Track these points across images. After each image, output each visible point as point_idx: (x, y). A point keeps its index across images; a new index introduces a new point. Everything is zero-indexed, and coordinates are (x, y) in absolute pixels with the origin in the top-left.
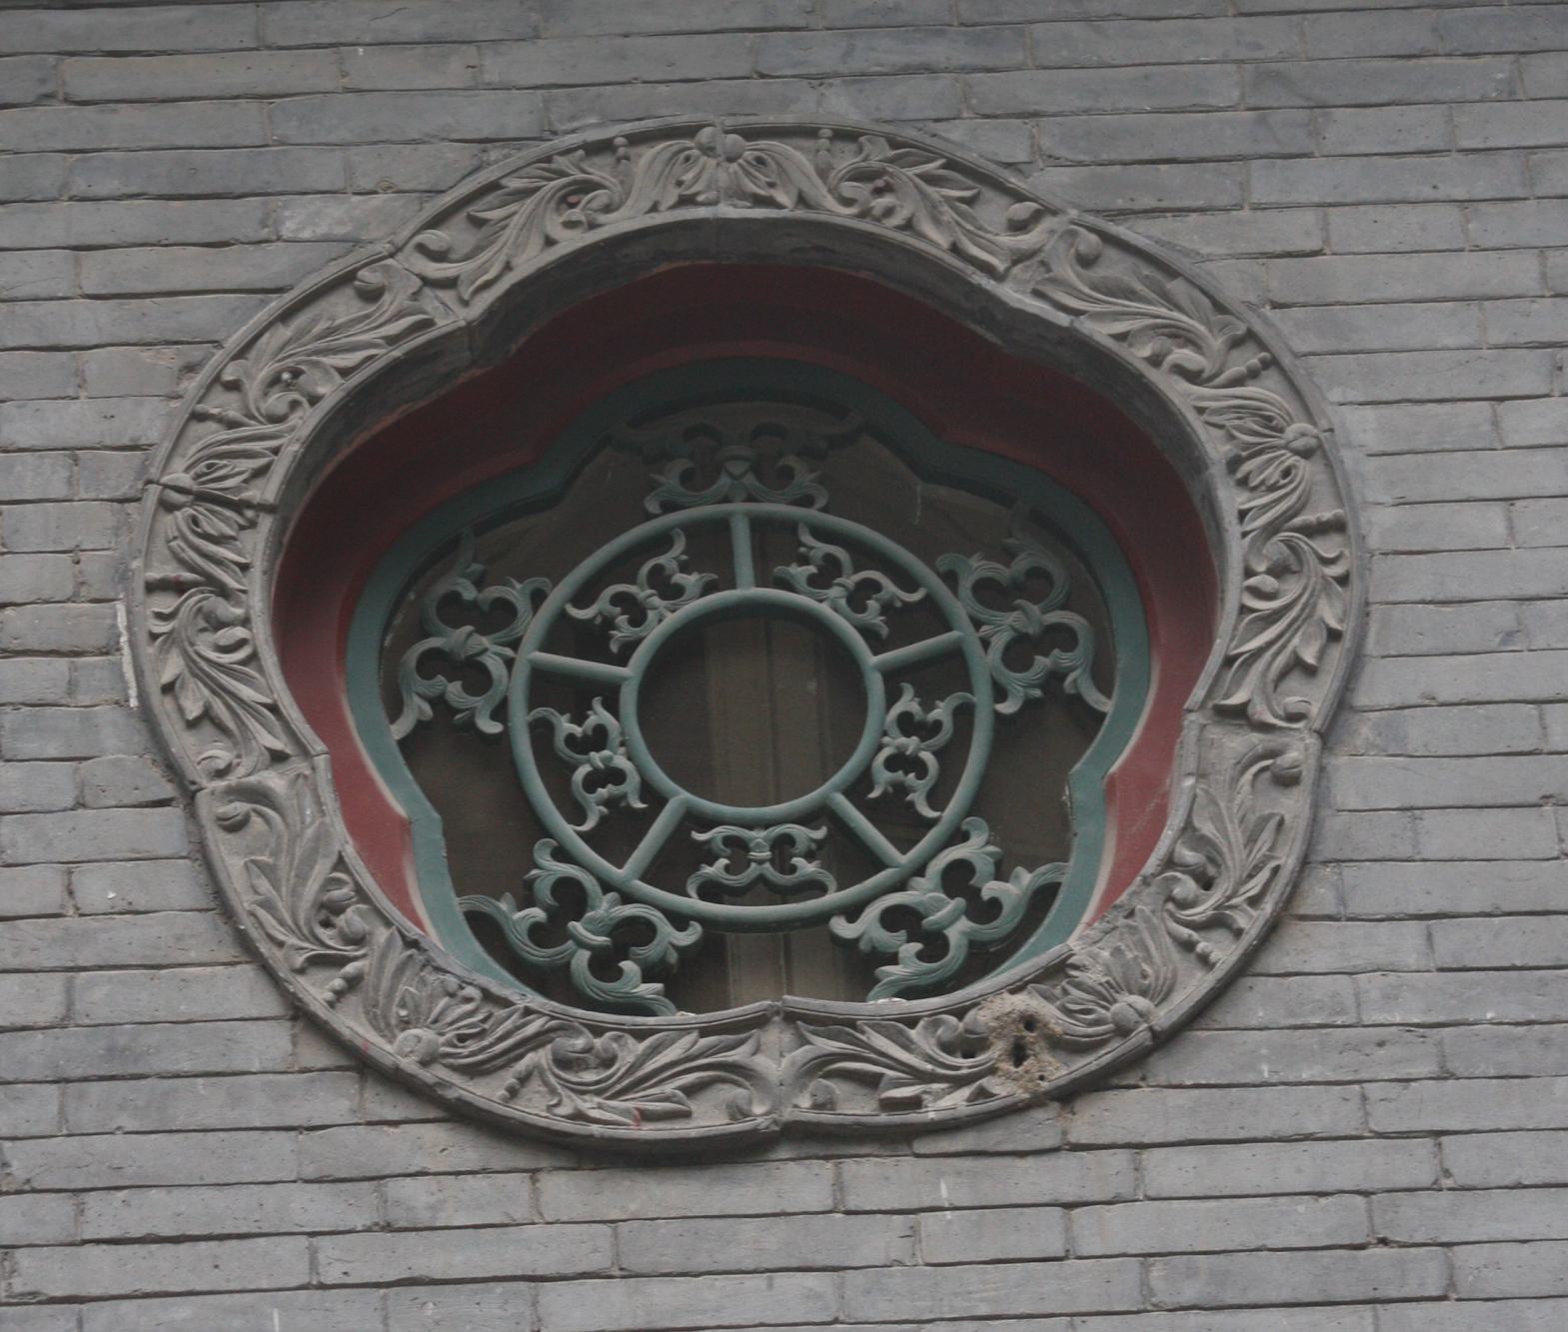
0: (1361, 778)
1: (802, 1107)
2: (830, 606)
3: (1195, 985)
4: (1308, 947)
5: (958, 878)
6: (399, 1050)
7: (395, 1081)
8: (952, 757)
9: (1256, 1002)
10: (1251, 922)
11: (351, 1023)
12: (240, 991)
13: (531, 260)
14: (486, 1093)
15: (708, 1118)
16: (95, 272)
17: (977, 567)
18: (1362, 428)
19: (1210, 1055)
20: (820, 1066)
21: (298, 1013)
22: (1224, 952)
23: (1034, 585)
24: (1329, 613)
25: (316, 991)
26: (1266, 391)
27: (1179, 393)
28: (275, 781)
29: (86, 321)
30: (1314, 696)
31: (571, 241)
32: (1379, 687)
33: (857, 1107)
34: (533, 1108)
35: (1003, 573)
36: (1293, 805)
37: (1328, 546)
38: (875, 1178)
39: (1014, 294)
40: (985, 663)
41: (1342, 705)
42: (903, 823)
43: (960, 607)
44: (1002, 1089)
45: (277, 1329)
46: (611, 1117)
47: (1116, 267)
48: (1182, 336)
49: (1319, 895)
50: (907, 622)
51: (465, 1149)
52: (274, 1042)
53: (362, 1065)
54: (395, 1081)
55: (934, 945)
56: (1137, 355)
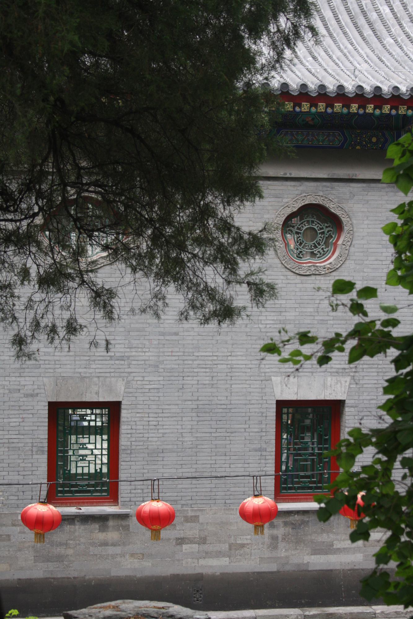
0: (352, 249)
1: (314, 273)
2: (315, 227)
3: (340, 265)
4: (347, 262)
5: (322, 249)
6: (288, 267)
7: (288, 269)
8: (323, 240)
9: (343, 266)
10: (343, 260)
11: (286, 265)
12: (277, 261)
13: (300, 205)
14: (294, 270)
15: (308, 273)
16: (270, 204)
17: (326, 225)
18: (355, 222)
19: (340, 270)
20: (315, 269)
21: (282, 263)
22: (342, 263)
23: (329, 227)
24: (351, 237)
25: (283, 262)
26: (348, 219)
27: (343, 219)
28: (281, 246)
29: (270, 208)
30: (349, 244)
31: (303, 204)
32: (353, 243)
33: (317, 273)
34: (297, 272)
35: (327, 225)
36: (347, 252)
37: (351, 232)
38: (318, 277)
39: (332, 211)
40: (326, 232)
41: (351, 244)
42: (319, 244)
43: (324, 228)
44: (327, 272)
45: (409, 368)
46: (302, 273)
47: (340, 209)
48: (343, 214)
49: (348, 258)
50: (321, 229)
51: (292, 274)
52: (280, 265)
53: (286, 267)
54: (288, 269)
55: (321, 254)
56: (340, 216)
